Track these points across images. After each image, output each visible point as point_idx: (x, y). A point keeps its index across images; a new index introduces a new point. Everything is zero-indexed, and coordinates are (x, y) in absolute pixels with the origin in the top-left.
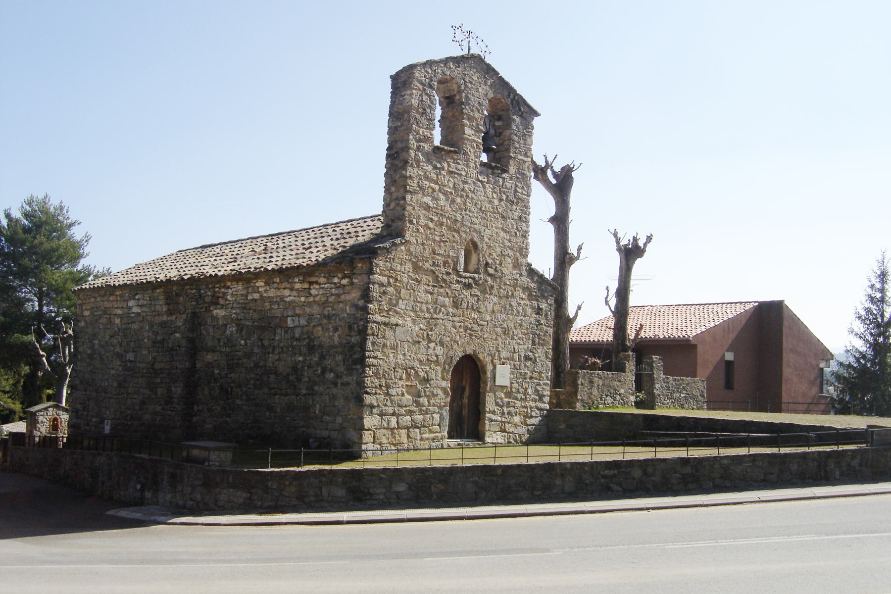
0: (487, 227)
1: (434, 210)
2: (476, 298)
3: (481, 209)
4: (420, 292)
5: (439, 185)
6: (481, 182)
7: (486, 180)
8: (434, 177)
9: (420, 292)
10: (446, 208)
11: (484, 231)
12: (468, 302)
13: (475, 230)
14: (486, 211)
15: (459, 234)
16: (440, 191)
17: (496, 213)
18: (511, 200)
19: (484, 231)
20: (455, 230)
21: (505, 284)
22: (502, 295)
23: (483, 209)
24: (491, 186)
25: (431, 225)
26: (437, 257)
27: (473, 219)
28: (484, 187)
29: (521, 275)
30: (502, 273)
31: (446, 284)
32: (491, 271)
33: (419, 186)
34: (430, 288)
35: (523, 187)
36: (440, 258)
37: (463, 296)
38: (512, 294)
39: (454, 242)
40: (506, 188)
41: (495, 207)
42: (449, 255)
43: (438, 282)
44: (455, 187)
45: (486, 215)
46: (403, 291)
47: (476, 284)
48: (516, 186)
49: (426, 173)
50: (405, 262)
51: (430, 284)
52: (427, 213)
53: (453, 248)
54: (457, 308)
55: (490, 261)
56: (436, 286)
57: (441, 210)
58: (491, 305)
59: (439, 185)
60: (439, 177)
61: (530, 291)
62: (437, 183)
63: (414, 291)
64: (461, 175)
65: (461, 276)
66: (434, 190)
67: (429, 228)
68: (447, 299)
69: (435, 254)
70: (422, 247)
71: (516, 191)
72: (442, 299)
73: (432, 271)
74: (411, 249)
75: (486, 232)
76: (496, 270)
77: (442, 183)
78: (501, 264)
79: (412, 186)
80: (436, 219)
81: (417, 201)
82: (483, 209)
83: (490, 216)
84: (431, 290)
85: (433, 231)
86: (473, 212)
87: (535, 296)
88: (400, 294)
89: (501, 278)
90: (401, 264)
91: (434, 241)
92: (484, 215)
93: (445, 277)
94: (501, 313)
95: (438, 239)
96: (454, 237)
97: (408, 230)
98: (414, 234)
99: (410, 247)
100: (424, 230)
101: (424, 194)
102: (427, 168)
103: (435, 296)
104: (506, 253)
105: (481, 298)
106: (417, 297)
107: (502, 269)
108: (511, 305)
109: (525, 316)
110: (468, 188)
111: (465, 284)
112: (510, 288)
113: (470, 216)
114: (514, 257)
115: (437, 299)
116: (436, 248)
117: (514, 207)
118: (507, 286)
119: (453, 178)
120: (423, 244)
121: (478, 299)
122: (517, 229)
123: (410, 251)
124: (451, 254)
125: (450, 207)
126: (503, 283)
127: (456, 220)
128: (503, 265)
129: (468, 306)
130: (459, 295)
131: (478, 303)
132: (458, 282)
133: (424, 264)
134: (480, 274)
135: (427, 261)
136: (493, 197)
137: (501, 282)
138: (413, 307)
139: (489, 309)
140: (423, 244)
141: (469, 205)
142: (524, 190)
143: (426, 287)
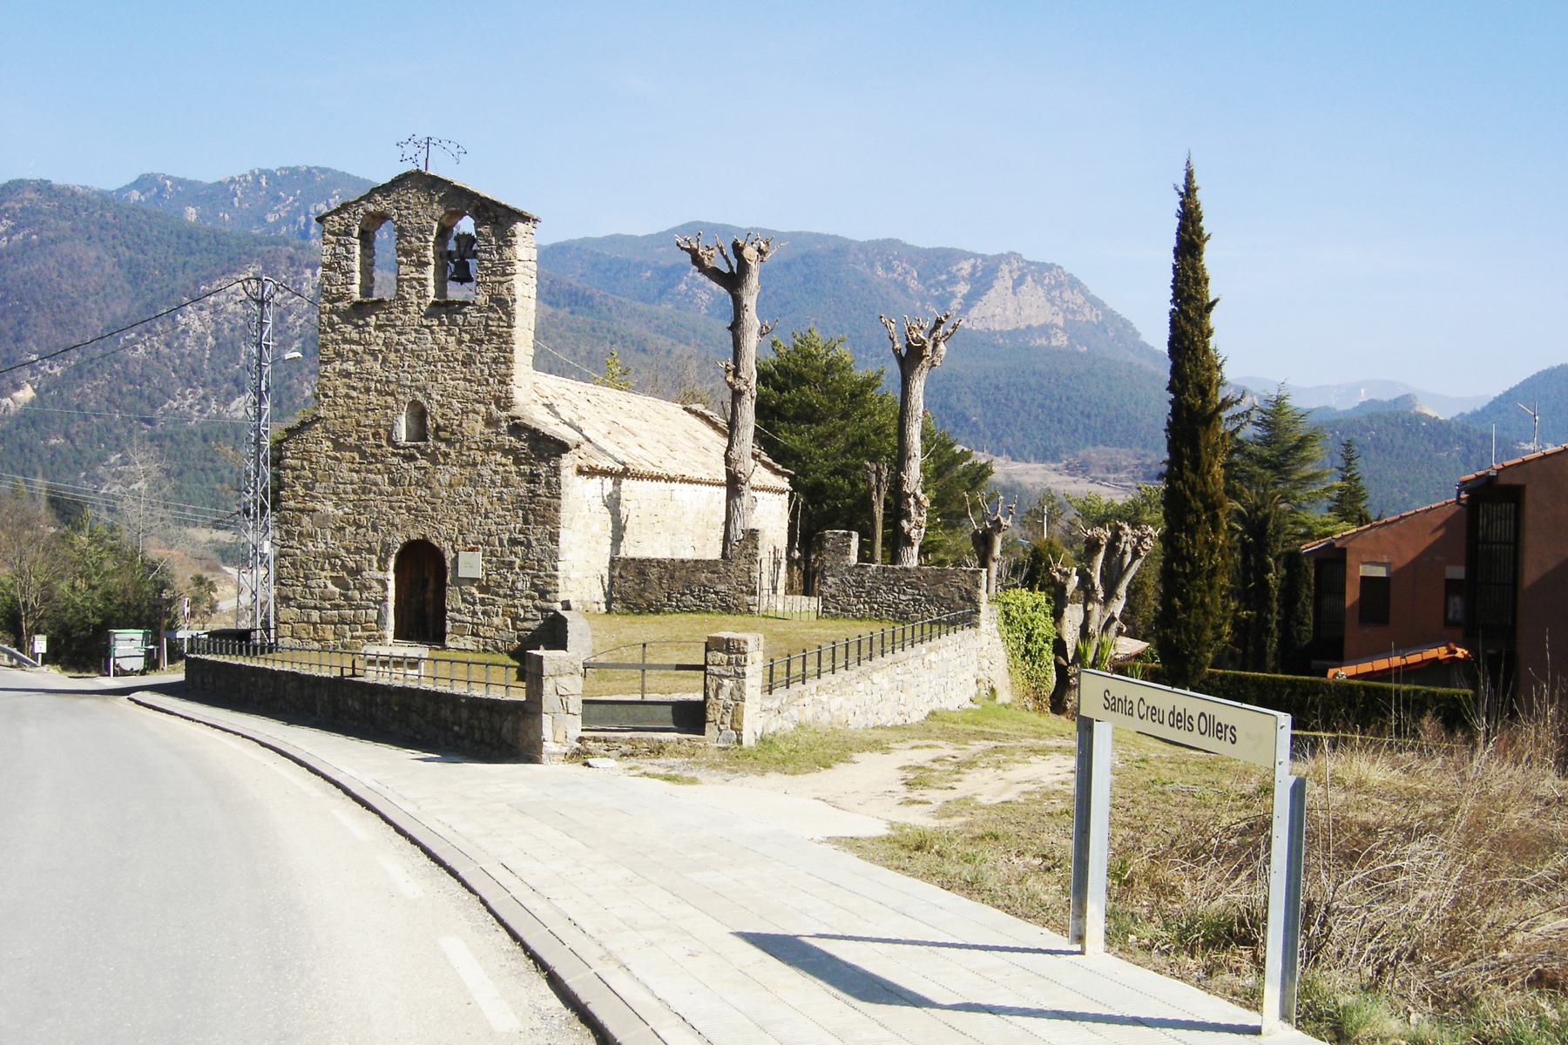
0: (436, 381)
2: (423, 472)
7: (436, 322)
16: (364, 352)
17: (450, 361)
18: (477, 339)
20: (388, 394)
21: (469, 449)
25: (354, 394)
27: (414, 375)
28: (432, 332)
29: (498, 434)
33: (335, 353)
34: (356, 466)
38: (483, 461)
39: (387, 408)
40: (470, 325)
42: (380, 426)
45: (435, 366)
46: (320, 472)
57: (368, 373)
58: (447, 476)
65: (398, 447)
66: (355, 353)
67: (352, 398)
71: (487, 325)
72: (372, 476)
78: (460, 425)
82: (431, 359)
83: (442, 366)
87: (525, 459)
90: (317, 444)
91: (358, 411)
92: (433, 367)
93: (374, 451)
95: (362, 408)
103: (363, 474)
105: (431, 470)
108: (480, 475)
109: (505, 487)
117: (484, 347)
119: (384, 332)
121: (426, 473)
127: (388, 382)
128: (464, 425)
132: (394, 454)
135: (350, 436)
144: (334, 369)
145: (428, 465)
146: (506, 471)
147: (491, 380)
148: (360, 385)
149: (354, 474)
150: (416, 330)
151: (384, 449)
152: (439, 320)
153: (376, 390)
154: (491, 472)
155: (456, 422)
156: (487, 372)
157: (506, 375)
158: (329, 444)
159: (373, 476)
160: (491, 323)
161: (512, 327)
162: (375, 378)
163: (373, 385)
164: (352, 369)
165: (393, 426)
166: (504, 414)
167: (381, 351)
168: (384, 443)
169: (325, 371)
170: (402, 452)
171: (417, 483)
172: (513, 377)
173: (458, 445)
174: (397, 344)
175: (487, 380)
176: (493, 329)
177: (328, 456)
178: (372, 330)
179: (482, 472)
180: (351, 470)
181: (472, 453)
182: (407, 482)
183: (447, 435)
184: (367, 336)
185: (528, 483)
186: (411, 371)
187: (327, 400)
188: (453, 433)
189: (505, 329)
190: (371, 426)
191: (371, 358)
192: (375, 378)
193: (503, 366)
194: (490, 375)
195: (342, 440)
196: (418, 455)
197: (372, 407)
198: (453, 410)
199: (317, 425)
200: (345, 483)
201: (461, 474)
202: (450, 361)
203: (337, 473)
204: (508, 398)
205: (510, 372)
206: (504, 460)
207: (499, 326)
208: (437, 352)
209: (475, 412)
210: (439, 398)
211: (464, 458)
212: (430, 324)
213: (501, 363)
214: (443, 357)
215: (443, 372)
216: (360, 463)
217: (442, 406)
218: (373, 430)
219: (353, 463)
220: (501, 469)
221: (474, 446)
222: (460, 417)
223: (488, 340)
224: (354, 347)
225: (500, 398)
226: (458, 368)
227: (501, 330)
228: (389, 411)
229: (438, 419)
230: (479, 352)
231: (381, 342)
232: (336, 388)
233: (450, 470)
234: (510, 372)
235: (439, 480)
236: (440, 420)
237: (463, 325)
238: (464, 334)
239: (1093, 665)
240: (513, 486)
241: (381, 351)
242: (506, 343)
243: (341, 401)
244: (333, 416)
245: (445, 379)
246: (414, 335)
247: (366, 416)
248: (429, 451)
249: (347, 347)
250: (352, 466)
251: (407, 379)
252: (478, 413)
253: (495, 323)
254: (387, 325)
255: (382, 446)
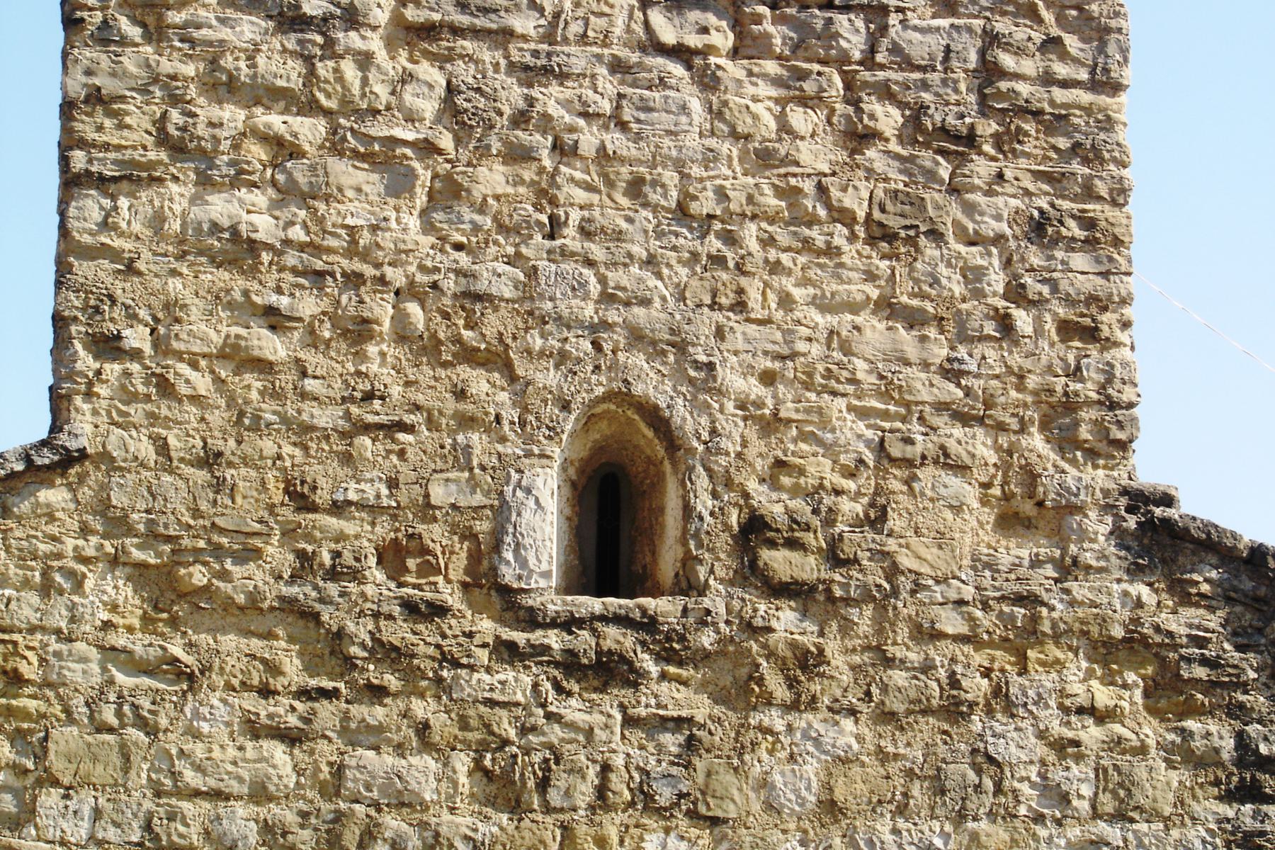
0: (740, 306)
1: (291, 259)
2: (672, 741)
3: (682, 212)
4: (197, 735)
5: (327, 113)
6: (680, 53)
7: (723, 39)
8: (290, 74)
9: (197, 735)
10: (385, 239)
11: (720, 333)
12: (606, 768)
13: (637, 337)
14: (728, 216)
15: (513, 378)
16: (335, 146)
17: (812, 221)
18: (944, 131)
19: (720, 333)
20: (469, 356)
21: (928, 634)
22: (899, 707)
23: (706, 204)
24: (771, 67)
25: (273, 346)
26: (332, 522)
27: (614, 277)
28: (708, 82)
29: (1068, 569)
30: (893, 571)
31: (411, 675)
32: (780, 562)
33: (163, 139)
34: (285, 711)
35: (1052, 44)
36: (350, 528)
37: (556, 733)
38: (999, 692)
39: (466, 422)
40: (908, 64)
41: (808, 186)
42: (426, 509)
43: (349, 663)
44: (457, 112)
45: (730, 239)
46: (66, 738)
47: (666, 656)
48: (991, 39)
49: (214, 62)
50: (70, 574)
51: (278, 683)
52: (239, 283)
53: (461, 459)
54: (516, 807)
55: (773, 505)
56: (332, 694)
57: (352, 250)
58: (811, 768)
59: (327, 113)
60: (324, 69)
61: (1162, 662)
62: (311, 108)
63: (151, 730)
64: (507, 34)
65: (532, 620)
66: (284, 149)
67: (263, 366)
68: (429, 762)
69: (314, 508)
70: (201, 476)
71: (989, 72)
72: (383, 762)
73: (289, 606)
74: (117, 498)
75: (736, 340)
76: (834, 556)
77: (346, 101)
78: (876, 519)
79: (106, 147)
80: (308, 305)
81: (158, 220)
82: (706, 204)
83: (768, 242)
84: (293, 721)
85: (286, 379)
86: (619, 236)
87: (1210, 686)
88: (41, 753)
89: (882, 602)
90: (47, 588)
91: (303, 431)
92: (714, 244)
93: (399, 632)
94: (902, 810)
95: (326, 417)
96: (461, 394)
97: (89, 395)
98: (137, 412)
99: (104, 487)
100: (219, 381)
101: (205, 182)
102: (225, 33)
103: (326, 751)
104: (922, 444)
105: (720, 736)
106: (179, 765)
107: (892, 545)
108: (986, 761)
109: (1120, 816)
110: (566, 104)
111: (570, 664)
112: (980, 659)
113: (590, 263)
114: (1005, 467)
115: (339, 771)
116: (314, 471)
117: (981, 169)
118: (948, 647)
119: (442, 60)
120: (210, 459)
121: (691, 744)
122: (1016, 293)
123: (109, 506)
124: (439, 494)
125: (428, 227)
126: (903, 632)
127: (473, 297)
128: (895, 522)
129: (602, 791)
130: (524, 731)
131: (688, 766)
132: (508, 652)
133: (224, 575)
134: (702, 590)
135: (250, 554)
136: (785, 128)
137: (882, 623)
138: (148, 827)
139: (787, 798)
140: (210, 459)
141: (581, 195)
142: (1064, 56)
143: (250, 702)
144: (158, 220)
145: (701, 708)
146: (1117, 743)
147: (1023, 320)
148: (308, 305)
149: (278, 751)
150: (617, 67)
151: (453, 625)
152: (738, 25)
153: (403, 335)
154: (1041, 750)
155: (850, 508)
156: (997, 280)
157: (1100, 303)
158: (125, 593)
159: (389, 760)
160: (1007, 60)
161: (1116, 88)
162: (396, 276)
163: (382, 310)
164: (264, 226)
165: (502, 512)
166: (1098, 477)
167: (428, 148)
168: (451, 596)
169: (105, 225)
170: (554, 640)
171: (644, 798)
172: (1128, 311)
173: (863, 619)
174: (520, 119)
175: (1005, 324)
176: (1023, 88)
177: (109, 652)
178: (375, 44)
179: (998, 749)
180: (254, 729)
181: (939, 654)
182: (584, 792)
183: (804, 566)
184: (349, 70)
185: (1229, 797)
186: (597, 251)
187: (113, 369)
188: (834, 556)
189: (1085, 97)
190: (374, 510)
191: (372, 182)
192: (396, 276)
193: (1080, 261)
194: (1016, 293)
195: (198, 576)
196: (649, 664)
197: (376, 413)
198: (830, 450)
199: (54, 496)
200: (217, 795)
201: (883, 756)
202: (812, 221)
203: (172, 742)
204: (1113, 405)
205: (1117, 286)
206: (1104, 696)
207: (1048, 79)
208: (739, 183)
209: (945, 460)
210: (756, 389)
211: (899, 677)
212: (694, 41)
213: (1071, 244)
214: (771, 201)
215: (775, 268)
216: (304, 694)
217: (771, 425)
218: (383, 530)
219: (266, 692)
220: (1091, 734)
221: (951, 623)
222: (866, 481)
223: (998, 141)
224: (275, 121)
225: (1070, 405)
226: (850, 254)
227: (1059, 95)
228: (476, 439)
229: (752, 485)
230: (954, 190)
231: (428, 107)
232: (172, 310)
233: (829, 735)
234: (1117, 286)
235: (764, 784)
236: (761, 495)
237: (869, 61)
238: (873, 105)
239: (922, 464)
240: (1152, 815)
241: (428, 148)
242: (1093, 156)
243: (202, 383)
244: (147, 450)
245: (786, 301)
246: (609, 84)
247: (347, 459)
248: (707, 639)
249: (233, 115)
250: (263, 709)
251: (579, 288)
252: (961, 469)
253: (1029, 66)
254: (457, 31)
255: (439, 610)
